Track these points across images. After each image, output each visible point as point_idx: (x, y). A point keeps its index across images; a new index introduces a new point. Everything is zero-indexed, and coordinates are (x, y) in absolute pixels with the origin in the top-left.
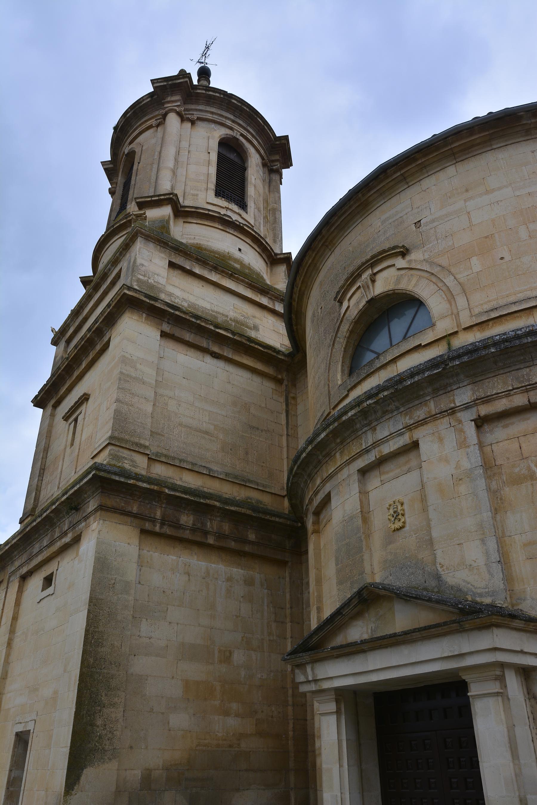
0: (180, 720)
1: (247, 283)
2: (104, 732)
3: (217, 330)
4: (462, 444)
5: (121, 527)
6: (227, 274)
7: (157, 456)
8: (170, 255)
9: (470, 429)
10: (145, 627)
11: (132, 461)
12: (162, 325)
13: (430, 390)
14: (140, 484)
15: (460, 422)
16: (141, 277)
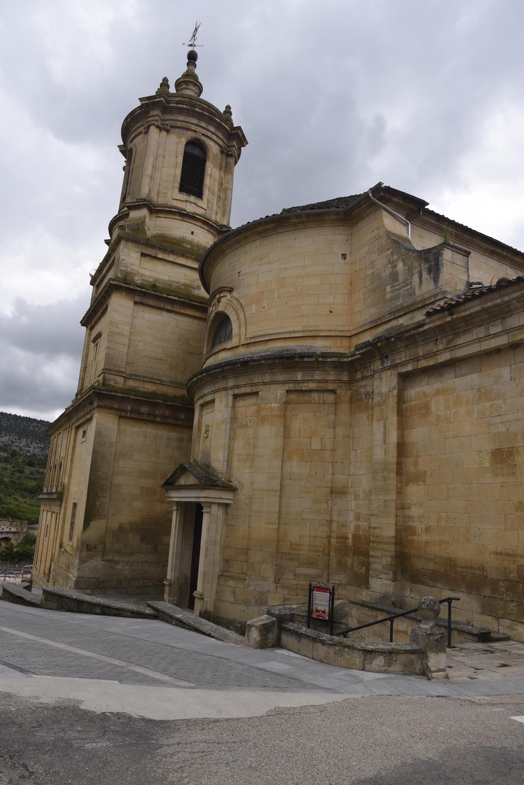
0: (138, 504)
1: (194, 258)
2: (100, 508)
3: (169, 297)
4: (227, 406)
5: (109, 415)
6: (180, 254)
7: (130, 376)
8: (142, 248)
9: (231, 398)
10: (121, 463)
11: (115, 381)
12: (135, 298)
13: (220, 376)
14: (117, 394)
15: (228, 395)
16: (123, 268)
